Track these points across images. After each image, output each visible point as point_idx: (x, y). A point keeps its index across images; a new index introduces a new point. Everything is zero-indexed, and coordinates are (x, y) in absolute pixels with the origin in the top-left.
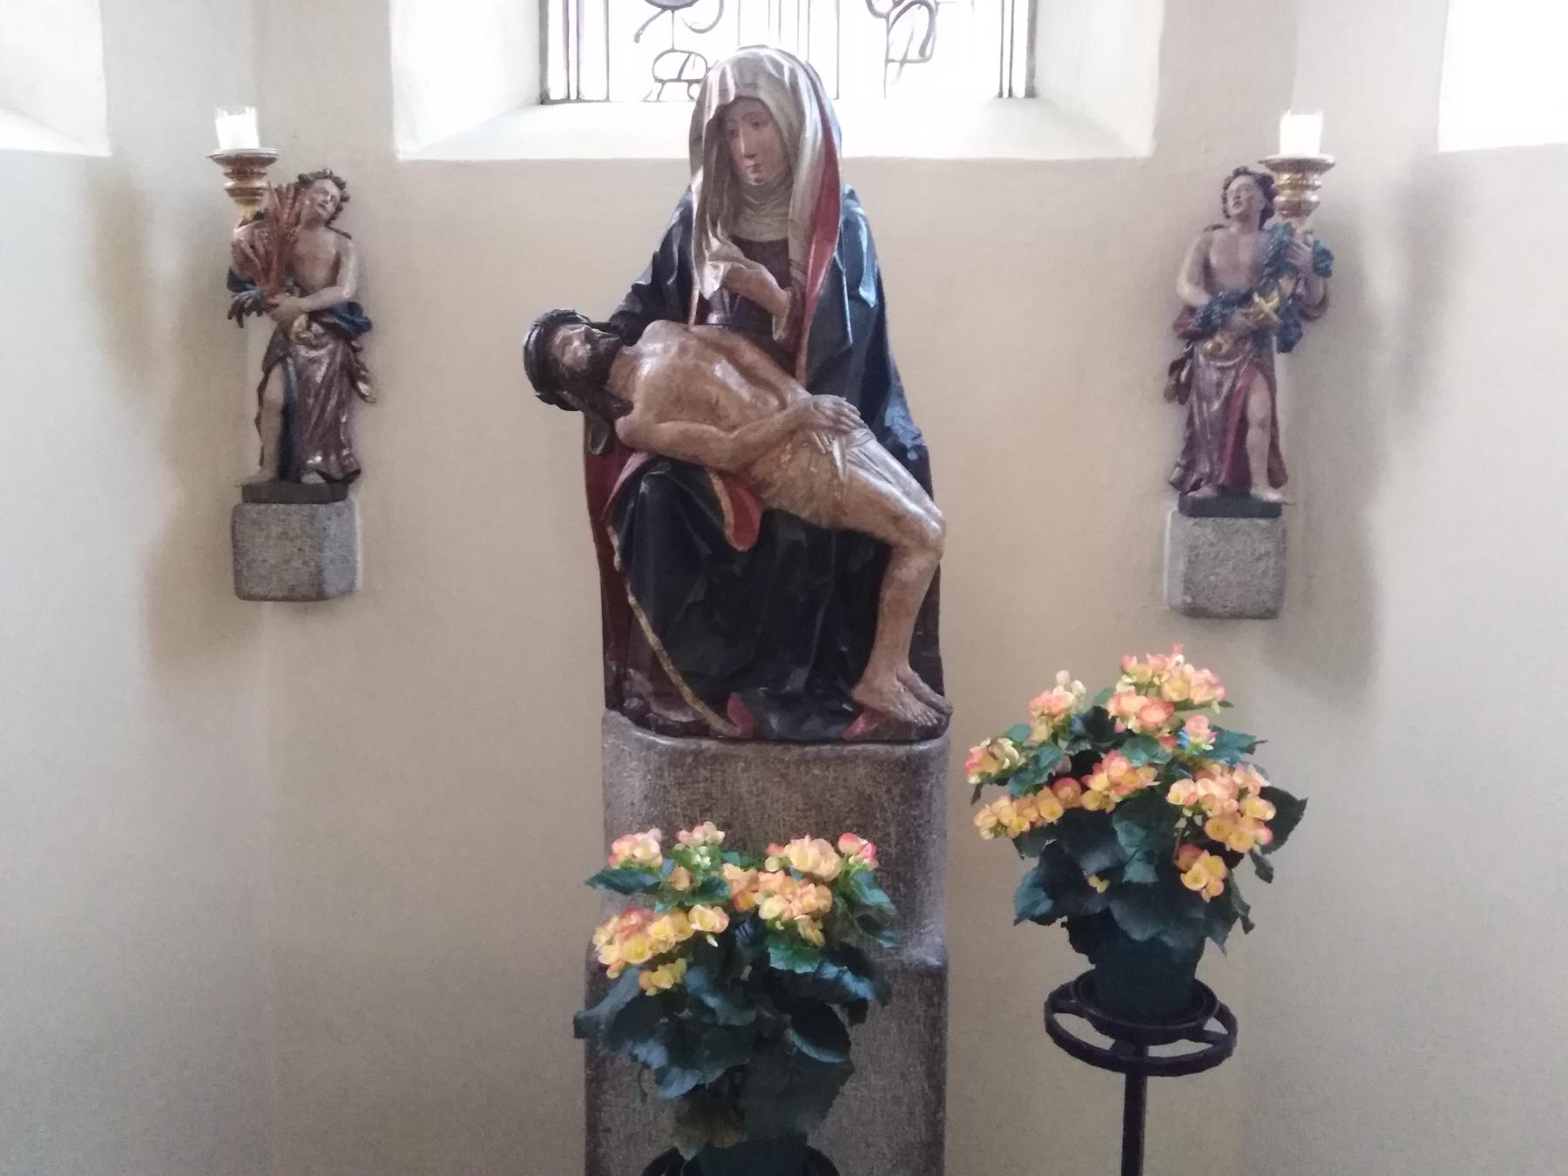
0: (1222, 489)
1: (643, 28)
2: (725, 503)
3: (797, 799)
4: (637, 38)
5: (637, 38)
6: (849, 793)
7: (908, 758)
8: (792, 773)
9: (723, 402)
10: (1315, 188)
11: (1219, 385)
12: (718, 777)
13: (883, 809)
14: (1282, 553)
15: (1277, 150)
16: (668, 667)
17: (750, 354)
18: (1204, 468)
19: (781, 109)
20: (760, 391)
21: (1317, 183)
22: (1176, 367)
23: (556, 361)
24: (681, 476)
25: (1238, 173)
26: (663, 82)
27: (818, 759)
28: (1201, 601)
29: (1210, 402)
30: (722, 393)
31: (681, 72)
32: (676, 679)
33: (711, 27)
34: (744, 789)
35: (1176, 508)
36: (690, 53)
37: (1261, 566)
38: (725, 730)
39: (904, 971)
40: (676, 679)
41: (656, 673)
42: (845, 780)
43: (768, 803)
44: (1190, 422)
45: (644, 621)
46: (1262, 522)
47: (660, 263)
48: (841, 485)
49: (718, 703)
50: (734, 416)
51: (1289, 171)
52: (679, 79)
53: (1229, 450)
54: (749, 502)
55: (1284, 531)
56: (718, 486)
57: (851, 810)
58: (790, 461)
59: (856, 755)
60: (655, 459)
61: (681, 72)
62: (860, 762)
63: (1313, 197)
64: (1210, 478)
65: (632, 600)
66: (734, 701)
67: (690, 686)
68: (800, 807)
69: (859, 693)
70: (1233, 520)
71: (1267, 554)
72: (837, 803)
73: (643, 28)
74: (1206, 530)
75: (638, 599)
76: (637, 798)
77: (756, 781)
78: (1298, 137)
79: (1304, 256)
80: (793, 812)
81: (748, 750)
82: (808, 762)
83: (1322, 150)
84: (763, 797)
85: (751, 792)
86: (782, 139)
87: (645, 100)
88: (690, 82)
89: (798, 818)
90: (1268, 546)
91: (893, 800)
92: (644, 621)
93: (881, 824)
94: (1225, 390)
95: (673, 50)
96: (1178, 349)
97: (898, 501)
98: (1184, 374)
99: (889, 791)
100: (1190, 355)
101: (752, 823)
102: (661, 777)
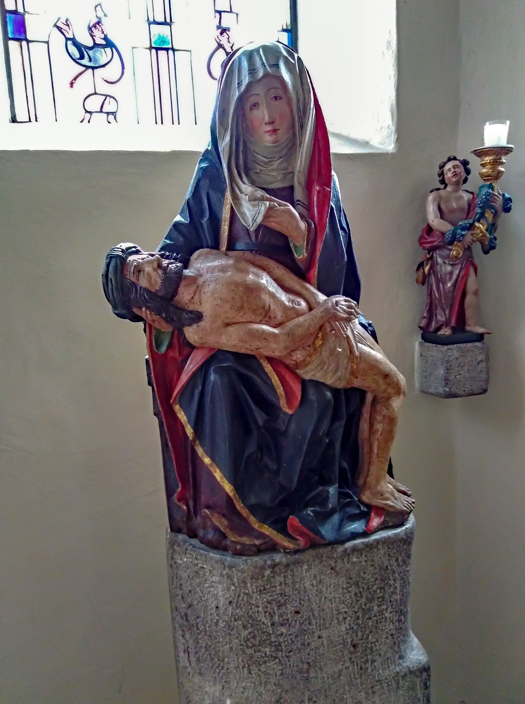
0: (454, 329)
1: (75, 79)
3: (342, 581)
5: (72, 84)
6: (375, 568)
7: (406, 534)
8: (339, 565)
9: (273, 307)
10: (502, 163)
11: (451, 273)
12: (289, 581)
13: (394, 572)
16: (239, 506)
17: (280, 271)
18: (441, 317)
19: (294, 87)
22: (421, 265)
24: (241, 369)
26: (90, 113)
27: (355, 549)
29: (444, 284)
31: (102, 107)
32: (245, 512)
34: (307, 585)
36: (106, 96)
37: (480, 367)
38: (291, 546)
39: (411, 672)
40: (245, 512)
41: (229, 509)
42: (372, 561)
43: (324, 589)
45: (218, 475)
46: (477, 344)
50: (279, 316)
52: (101, 111)
53: (456, 308)
54: (288, 377)
55: (488, 348)
56: (268, 368)
57: (376, 579)
58: (322, 344)
59: (377, 542)
60: (216, 356)
61: (102, 107)
62: (380, 546)
64: (447, 323)
65: (207, 460)
66: (293, 520)
68: (345, 586)
71: (482, 361)
72: (368, 577)
73: (75, 79)
75: (213, 459)
77: (315, 577)
79: (499, 203)
80: (340, 590)
83: (507, 143)
84: (320, 587)
85: (313, 585)
87: (82, 122)
88: (108, 113)
89: (343, 594)
91: (398, 565)
92: (218, 475)
93: (392, 582)
94: (455, 277)
95: (95, 93)
96: (422, 255)
97: (387, 364)
99: (397, 560)
100: (432, 258)
101: (314, 606)
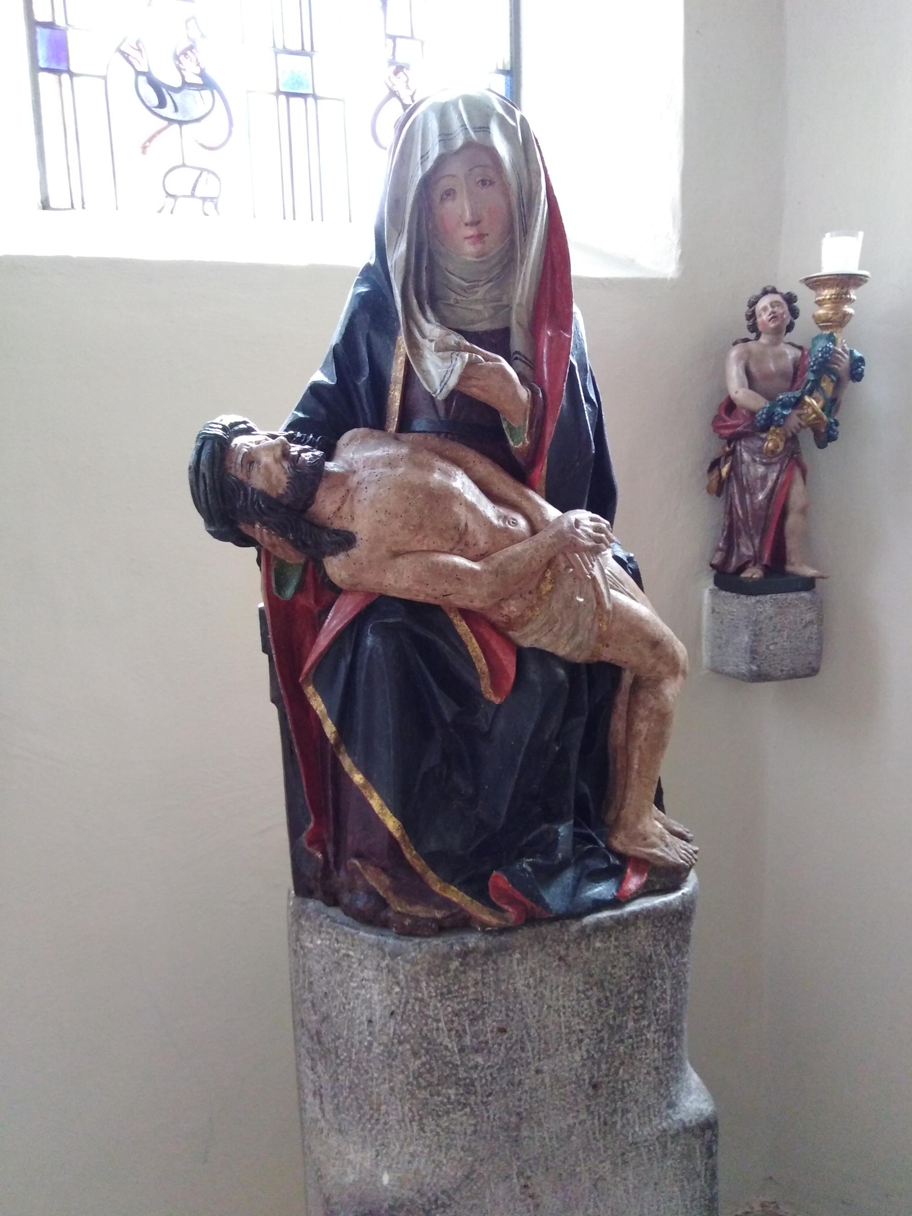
0: (767, 569)
2: (474, 648)
3: (577, 980)
4: (144, 148)
6: (631, 959)
9: (472, 526)
11: (764, 478)
13: (661, 965)
14: (820, 620)
15: (820, 269)
16: (410, 854)
17: (485, 468)
20: (503, 511)
21: (853, 297)
22: (715, 464)
23: (241, 485)
25: (765, 292)
28: (765, 667)
29: (753, 494)
30: (470, 516)
32: (419, 865)
33: (165, 177)
35: (712, 586)
36: (202, 170)
37: (807, 633)
40: (419, 865)
43: (547, 993)
44: (730, 512)
46: (804, 594)
47: (344, 356)
48: (608, 612)
49: (478, 888)
50: (482, 540)
51: (831, 287)
52: (193, 195)
54: (495, 643)
56: (462, 627)
57: (633, 977)
59: (636, 915)
63: (848, 309)
65: (358, 778)
66: (499, 879)
67: (435, 871)
69: (619, 842)
70: (784, 596)
74: (738, 605)
75: (367, 775)
76: (378, 1011)
77: (533, 973)
78: (839, 255)
80: (574, 995)
81: (523, 936)
82: (589, 936)
83: (860, 269)
86: (509, 204)
89: (579, 1000)
90: (809, 616)
92: (376, 802)
94: (770, 484)
95: (184, 165)
98: (725, 470)
100: (733, 452)
102: (418, 988)
